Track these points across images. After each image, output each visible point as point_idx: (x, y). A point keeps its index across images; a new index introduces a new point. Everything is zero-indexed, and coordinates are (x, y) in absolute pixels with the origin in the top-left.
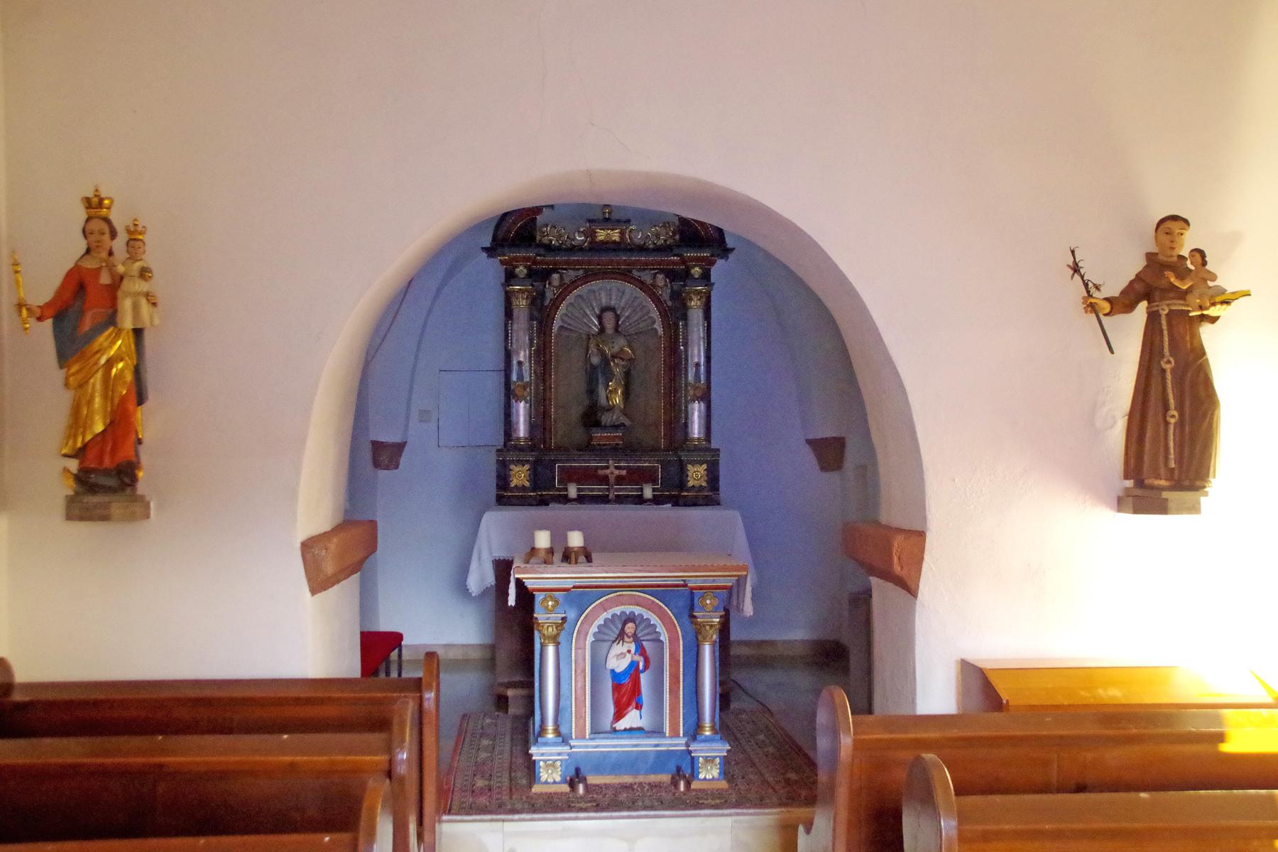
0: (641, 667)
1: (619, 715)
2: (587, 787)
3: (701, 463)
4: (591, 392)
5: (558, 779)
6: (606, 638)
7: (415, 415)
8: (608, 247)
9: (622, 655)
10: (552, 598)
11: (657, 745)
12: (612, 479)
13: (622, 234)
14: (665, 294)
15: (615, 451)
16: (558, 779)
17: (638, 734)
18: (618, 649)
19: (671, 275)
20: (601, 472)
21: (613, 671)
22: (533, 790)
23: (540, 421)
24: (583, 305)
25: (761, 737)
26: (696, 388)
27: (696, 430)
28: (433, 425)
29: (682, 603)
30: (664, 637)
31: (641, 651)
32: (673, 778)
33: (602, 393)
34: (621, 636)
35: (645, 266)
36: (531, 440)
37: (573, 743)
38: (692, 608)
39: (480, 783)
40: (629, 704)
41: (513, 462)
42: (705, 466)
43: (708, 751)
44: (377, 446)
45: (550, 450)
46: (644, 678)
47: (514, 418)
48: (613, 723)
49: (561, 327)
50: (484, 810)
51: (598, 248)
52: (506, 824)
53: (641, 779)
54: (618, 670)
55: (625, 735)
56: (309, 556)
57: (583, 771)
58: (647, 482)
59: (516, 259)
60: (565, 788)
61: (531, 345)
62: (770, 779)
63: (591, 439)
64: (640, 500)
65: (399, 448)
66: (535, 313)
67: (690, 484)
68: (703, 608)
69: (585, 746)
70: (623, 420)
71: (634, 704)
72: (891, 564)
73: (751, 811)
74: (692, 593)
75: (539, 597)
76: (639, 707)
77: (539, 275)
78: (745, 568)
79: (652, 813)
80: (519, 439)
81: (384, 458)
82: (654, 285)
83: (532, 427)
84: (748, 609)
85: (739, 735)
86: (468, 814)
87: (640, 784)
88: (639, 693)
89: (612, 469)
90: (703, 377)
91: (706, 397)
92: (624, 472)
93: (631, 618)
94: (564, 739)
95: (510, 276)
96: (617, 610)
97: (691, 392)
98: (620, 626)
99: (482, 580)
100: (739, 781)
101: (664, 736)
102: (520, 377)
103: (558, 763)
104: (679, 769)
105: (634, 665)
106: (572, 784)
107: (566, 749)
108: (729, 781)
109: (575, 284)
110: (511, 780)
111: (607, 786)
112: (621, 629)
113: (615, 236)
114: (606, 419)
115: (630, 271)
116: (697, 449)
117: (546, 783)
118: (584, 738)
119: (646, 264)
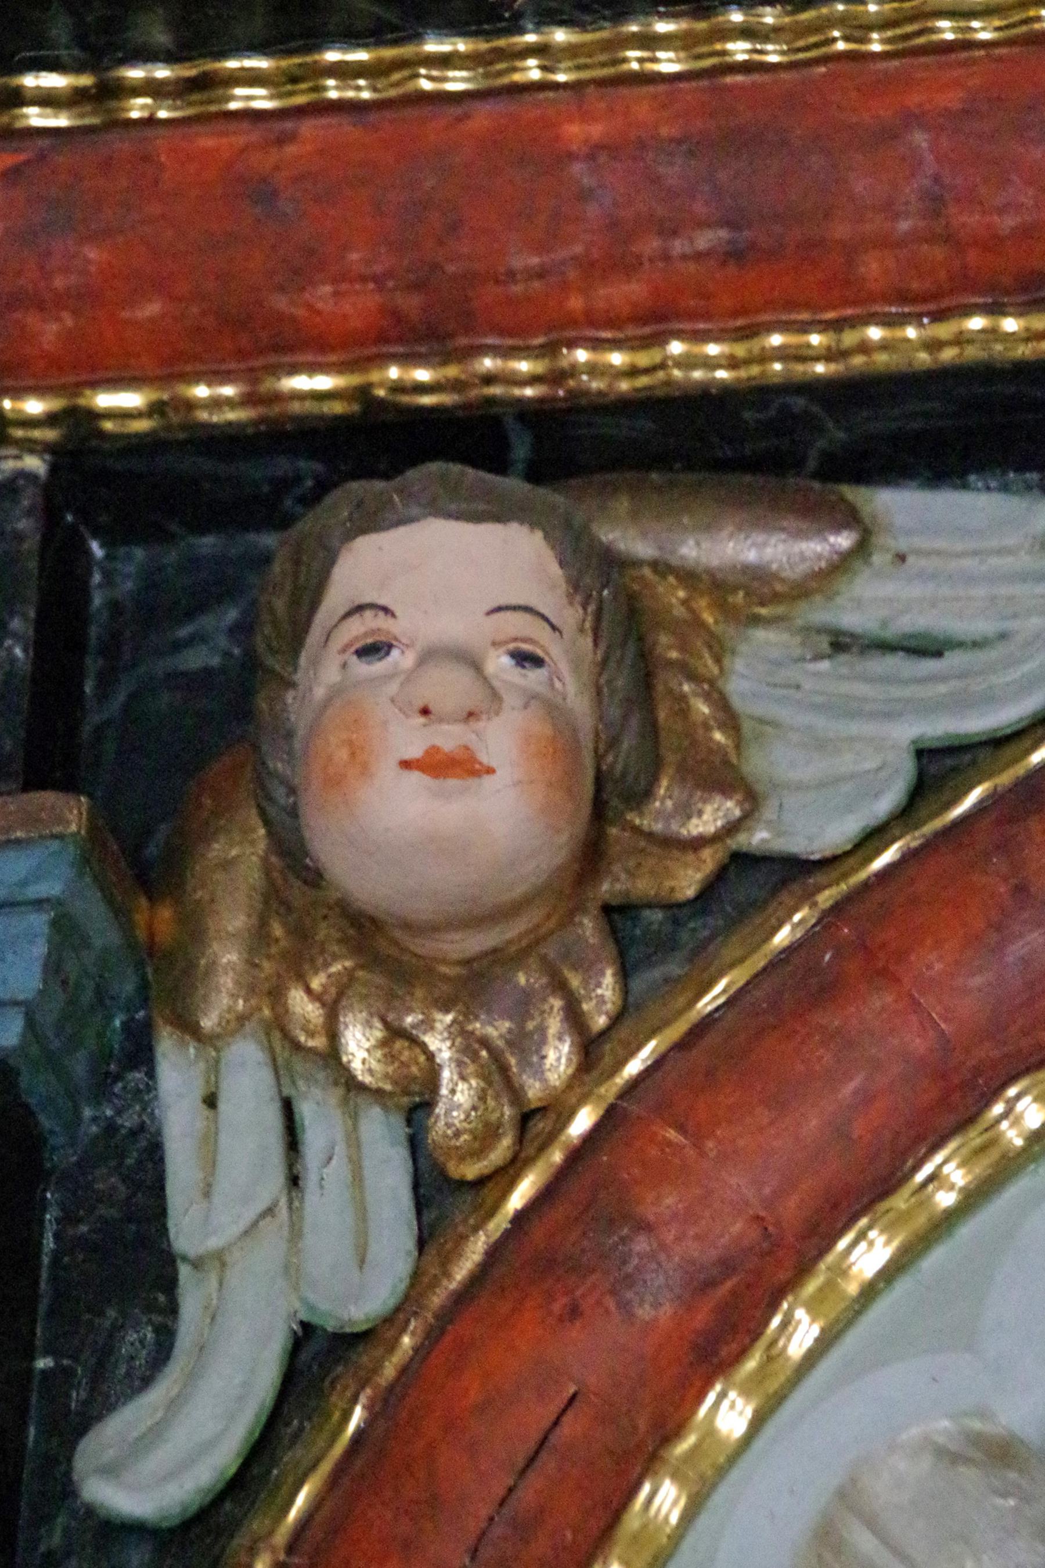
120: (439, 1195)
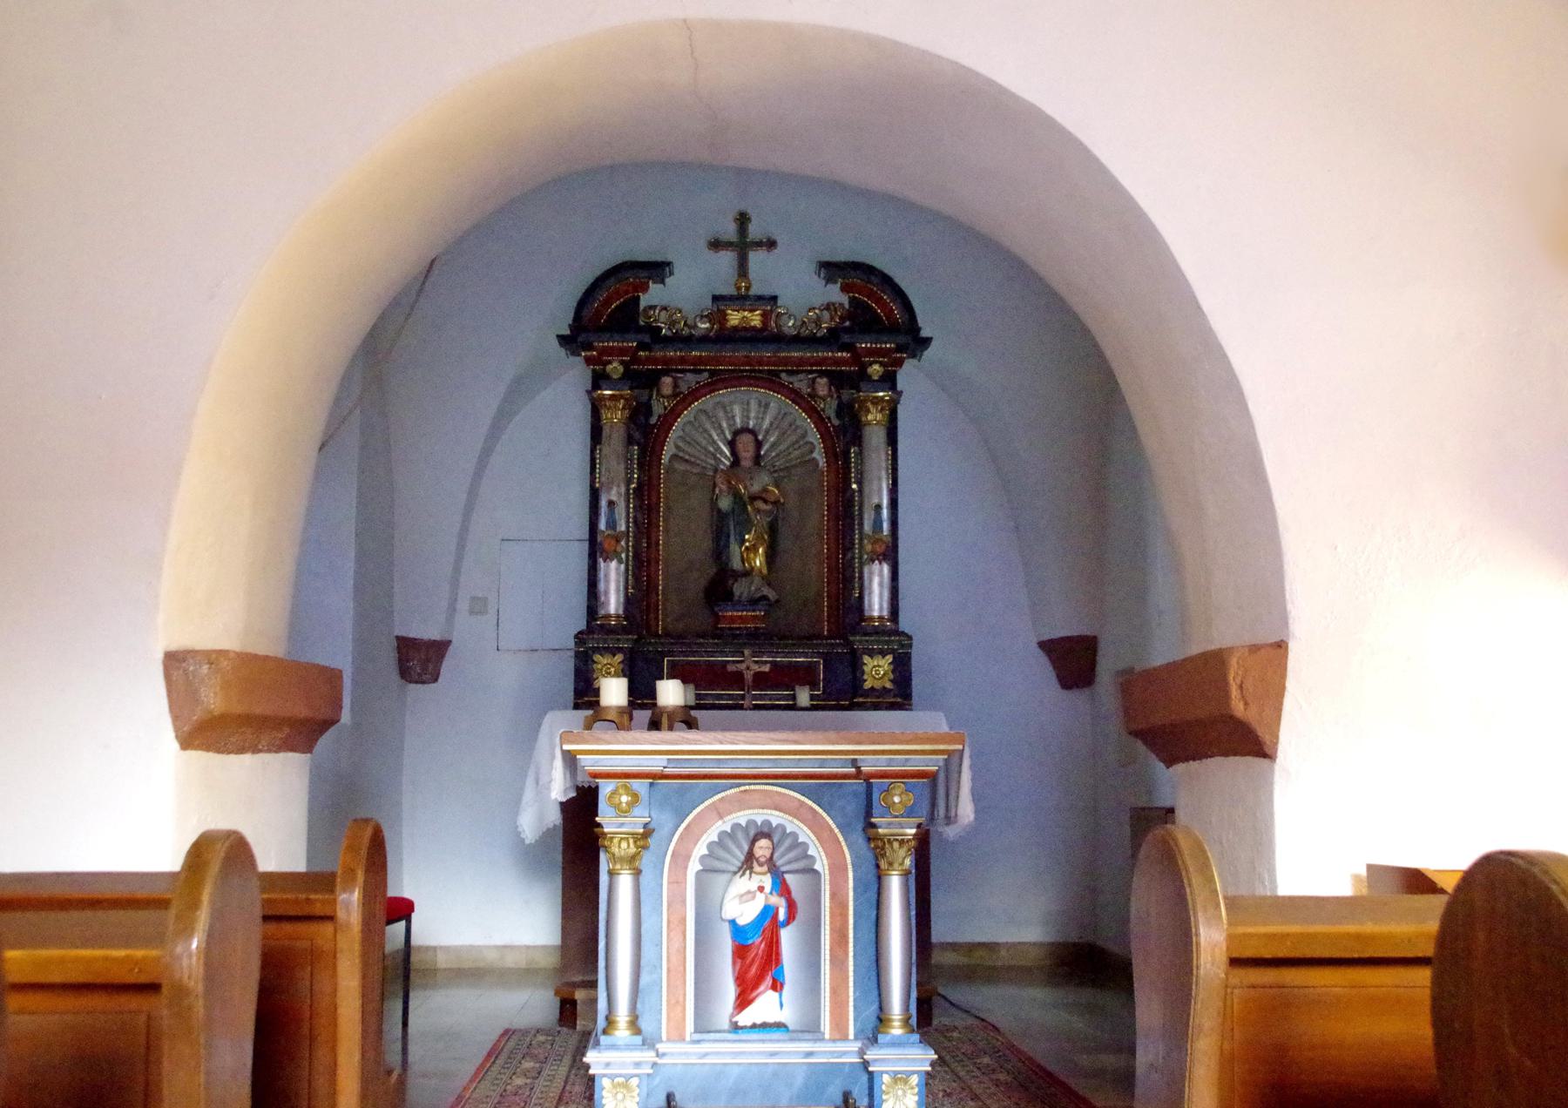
0: (782, 915)
1: (743, 1002)
3: (883, 653)
4: (719, 553)
7: (463, 605)
9: (750, 895)
10: (629, 791)
11: (809, 1054)
12: (748, 676)
13: (765, 316)
14: (829, 408)
15: (758, 639)
17: (776, 1035)
18: (744, 884)
19: (838, 380)
20: (731, 668)
21: (733, 922)
23: (640, 595)
25: (986, 1060)
26: (876, 541)
27: (876, 603)
28: (490, 617)
29: (854, 807)
30: (822, 865)
31: (783, 889)
33: (735, 550)
34: (749, 860)
35: (797, 368)
36: (626, 618)
37: (661, 1047)
38: (869, 813)
40: (759, 979)
42: (890, 658)
44: (406, 647)
45: (657, 635)
46: (787, 937)
47: (601, 586)
48: (733, 1016)
49: (674, 457)
51: (727, 337)
54: (741, 922)
55: (754, 1035)
56: (175, 674)
59: (610, 351)
61: (629, 482)
63: (717, 619)
64: (793, 708)
65: (438, 649)
66: (637, 435)
67: (867, 685)
68: (889, 807)
70: (766, 591)
71: (768, 981)
74: (869, 787)
75: (606, 788)
76: (777, 986)
77: (642, 379)
80: (608, 616)
81: (415, 665)
82: (813, 395)
83: (629, 602)
84: (966, 810)
88: (778, 961)
90: (886, 526)
91: (890, 554)
92: (766, 668)
93: (765, 832)
94: (649, 1043)
95: (599, 379)
96: (742, 817)
97: (869, 547)
98: (746, 848)
99: (541, 817)
101: (823, 1040)
102: (612, 524)
103: (634, 1082)
105: (769, 913)
107: (649, 1056)
109: (695, 394)
112: (754, 849)
113: (755, 320)
114: (740, 589)
115: (776, 374)
116: (877, 632)
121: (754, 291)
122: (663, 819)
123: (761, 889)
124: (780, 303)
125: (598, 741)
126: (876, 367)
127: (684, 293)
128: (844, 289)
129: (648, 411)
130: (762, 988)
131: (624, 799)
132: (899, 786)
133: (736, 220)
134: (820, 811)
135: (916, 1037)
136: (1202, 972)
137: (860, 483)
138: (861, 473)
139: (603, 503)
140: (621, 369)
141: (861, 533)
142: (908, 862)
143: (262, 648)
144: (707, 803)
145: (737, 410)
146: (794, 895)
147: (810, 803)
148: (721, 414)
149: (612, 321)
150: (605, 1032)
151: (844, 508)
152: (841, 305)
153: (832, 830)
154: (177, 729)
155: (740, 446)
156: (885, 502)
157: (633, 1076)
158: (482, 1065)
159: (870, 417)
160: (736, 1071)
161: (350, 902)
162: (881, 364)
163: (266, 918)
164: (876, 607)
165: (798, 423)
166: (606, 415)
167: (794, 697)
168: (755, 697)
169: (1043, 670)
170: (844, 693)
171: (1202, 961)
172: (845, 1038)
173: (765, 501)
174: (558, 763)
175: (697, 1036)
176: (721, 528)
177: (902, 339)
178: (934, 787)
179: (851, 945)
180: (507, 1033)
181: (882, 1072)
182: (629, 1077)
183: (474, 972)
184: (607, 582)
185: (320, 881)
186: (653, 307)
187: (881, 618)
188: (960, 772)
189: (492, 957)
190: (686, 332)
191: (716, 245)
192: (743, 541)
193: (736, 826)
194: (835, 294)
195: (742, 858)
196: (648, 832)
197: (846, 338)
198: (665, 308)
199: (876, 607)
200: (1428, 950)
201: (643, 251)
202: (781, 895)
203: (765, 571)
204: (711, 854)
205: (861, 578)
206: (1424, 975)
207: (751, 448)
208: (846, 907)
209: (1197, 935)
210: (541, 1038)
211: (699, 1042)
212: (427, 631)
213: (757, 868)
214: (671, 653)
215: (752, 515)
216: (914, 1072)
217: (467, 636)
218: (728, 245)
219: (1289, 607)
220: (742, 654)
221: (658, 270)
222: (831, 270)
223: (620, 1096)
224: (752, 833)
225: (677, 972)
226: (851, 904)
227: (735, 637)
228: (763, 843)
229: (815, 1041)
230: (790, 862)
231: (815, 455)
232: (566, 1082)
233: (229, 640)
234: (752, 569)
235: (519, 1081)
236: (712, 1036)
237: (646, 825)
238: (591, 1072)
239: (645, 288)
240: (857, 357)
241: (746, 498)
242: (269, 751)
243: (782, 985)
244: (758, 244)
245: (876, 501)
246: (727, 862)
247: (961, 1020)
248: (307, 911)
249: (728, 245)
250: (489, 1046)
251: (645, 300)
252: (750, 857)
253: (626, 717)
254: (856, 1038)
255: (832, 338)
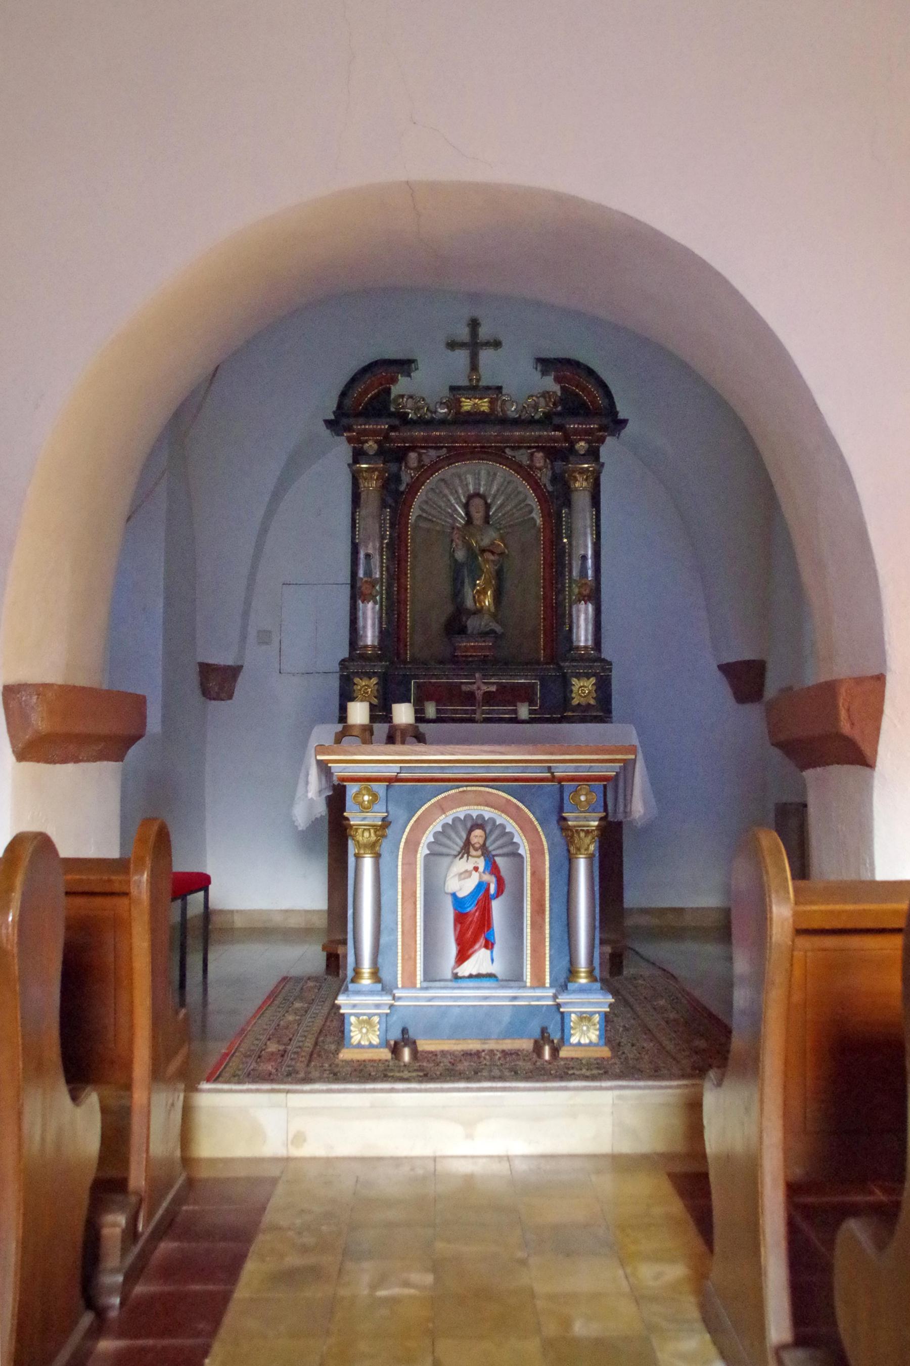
0: (493, 889)
1: (463, 956)
2: (415, 1053)
3: (588, 676)
4: (457, 594)
5: (375, 1041)
6: (445, 850)
8: (476, 419)
11: (515, 998)
12: (479, 695)
13: (492, 402)
14: (545, 477)
15: (486, 664)
16: (375, 1041)
18: (463, 865)
19: (553, 454)
20: (464, 688)
21: (454, 895)
22: (341, 1056)
24: (446, 491)
25: (662, 1002)
27: (583, 636)
29: (549, 804)
30: (524, 850)
31: (493, 869)
32: (536, 1042)
34: (466, 849)
36: (380, 649)
37: (398, 993)
38: (561, 809)
39: (273, 1047)
40: (475, 941)
41: (357, 674)
42: (593, 680)
43: (582, 1004)
44: (206, 670)
45: (405, 662)
46: (496, 907)
47: (361, 623)
48: (454, 968)
50: (268, 1078)
52: (290, 1096)
53: (491, 1045)
54: (461, 895)
55: (471, 983)
57: (412, 1034)
58: (523, 701)
59: (365, 432)
60: (386, 1054)
61: (382, 538)
62: (670, 1046)
64: (515, 720)
66: (390, 501)
67: (575, 702)
68: (577, 806)
69: (414, 998)
71: (482, 941)
72: (837, 718)
73: (641, 1083)
74: (561, 789)
75: (352, 789)
76: (489, 945)
77: (394, 455)
78: (632, 750)
79: (500, 1085)
80: (366, 646)
81: (213, 685)
82: (531, 467)
83: (383, 634)
85: (631, 1000)
86: (239, 1082)
87: (492, 1052)
89: (479, 712)
90: (590, 572)
91: (594, 596)
93: (479, 824)
94: (387, 989)
95: (358, 455)
96: (461, 812)
97: (576, 591)
98: (464, 836)
100: (627, 1049)
101: (525, 987)
102: (368, 573)
103: (376, 1019)
104: (544, 1030)
105: (482, 887)
106: (396, 1050)
107: (387, 999)
108: (612, 1049)
109: (434, 467)
110: (316, 1044)
111: (444, 1053)
112: (471, 837)
113: (484, 405)
114: (472, 624)
115: (502, 450)
116: (582, 658)
117: (359, 1046)
118: (413, 986)
119: (522, 440)
120: (412, 478)
121: (483, 383)
122: (398, 813)
123: (476, 869)
124: (504, 391)
125: (345, 753)
126: (582, 443)
127: (427, 384)
128: (558, 380)
129: (397, 479)
130: (477, 946)
131: (366, 798)
132: (585, 787)
133: (468, 325)
134: (523, 807)
135: (598, 985)
136: (774, 939)
137: (569, 537)
138: (570, 529)
139: (362, 555)
140: (375, 446)
141: (570, 578)
142: (592, 848)
143: (81, 680)
144: (433, 801)
145: (470, 479)
146: (503, 873)
147: (515, 801)
148: (457, 481)
149: (368, 406)
150: (353, 981)
151: (557, 558)
152: (555, 393)
153: (532, 822)
154: (13, 746)
155: (473, 510)
156: (590, 553)
157: (375, 1014)
158: (260, 1008)
159: (577, 485)
160: (457, 1010)
161: (141, 882)
162: (587, 441)
163: (67, 893)
164: (583, 638)
165: (520, 489)
166: (363, 484)
167: (515, 712)
168: (483, 712)
169: (723, 690)
170: (557, 709)
171: (774, 932)
172: (542, 985)
173: (493, 553)
174: (314, 772)
175: (425, 984)
176: (458, 575)
177: (605, 421)
178: (613, 787)
179: (547, 913)
180: (285, 979)
181: (571, 1013)
182: (370, 1016)
183: (264, 930)
184: (365, 619)
185: (120, 866)
186: (402, 396)
187: (586, 647)
188: (633, 776)
189: (278, 919)
190: (428, 416)
191: (452, 345)
192: (475, 585)
193: (456, 819)
194: (550, 384)
195: (461, 844)
196: (386, 823)
197: (557, 421)
198: (411, 397)
199: (583, 638)
200: (900, 923)
201: (392, 352)
202: (491, 873)
203: (492, 609)
204: (436, 842)
205: (571, 615)
206: (897, 941)
207: (482, 509)
208: (543, 883)
209: (771, 912)
210: (311, 984)
211: (427, 988)
212: (223, 658)
213: (473, 852)
214: (416, 677)
215: (482, 564)
216: (595, 1013)
217: (255, 659)
218: (462, 345)
219: (887, 647)
220: (473, 676)
221: (405, 365)
222: (546, 364)
223: (364, 1030)
224: (469, 825)
225: (409, 934)
226: (547, 880)
227: (468, 663)
228: (478, 832)
229: (520, 988)
230: (498, 848)
231: (534, 515)
232: (327, 1018)
233: (55, 677)
234: (482, 607)
235: (290, 1018)
236: (437, 984)
237: (384, 819)
238: (342, 1011)
239: (394, 380)
240: (566, 438)
241: (477, 552)
242: (88, 761)
243: (493, 944)
244: (487, 344)
245: (582, 552)
246: (449, 847)
247: (646, 971)
248: (107, 889)
249: (462, 345)
250: (271, 988)
251: (395, 390)
252: (467, 844)
253: (367, 733)
254: (551, 986)
255: (547, 420)
